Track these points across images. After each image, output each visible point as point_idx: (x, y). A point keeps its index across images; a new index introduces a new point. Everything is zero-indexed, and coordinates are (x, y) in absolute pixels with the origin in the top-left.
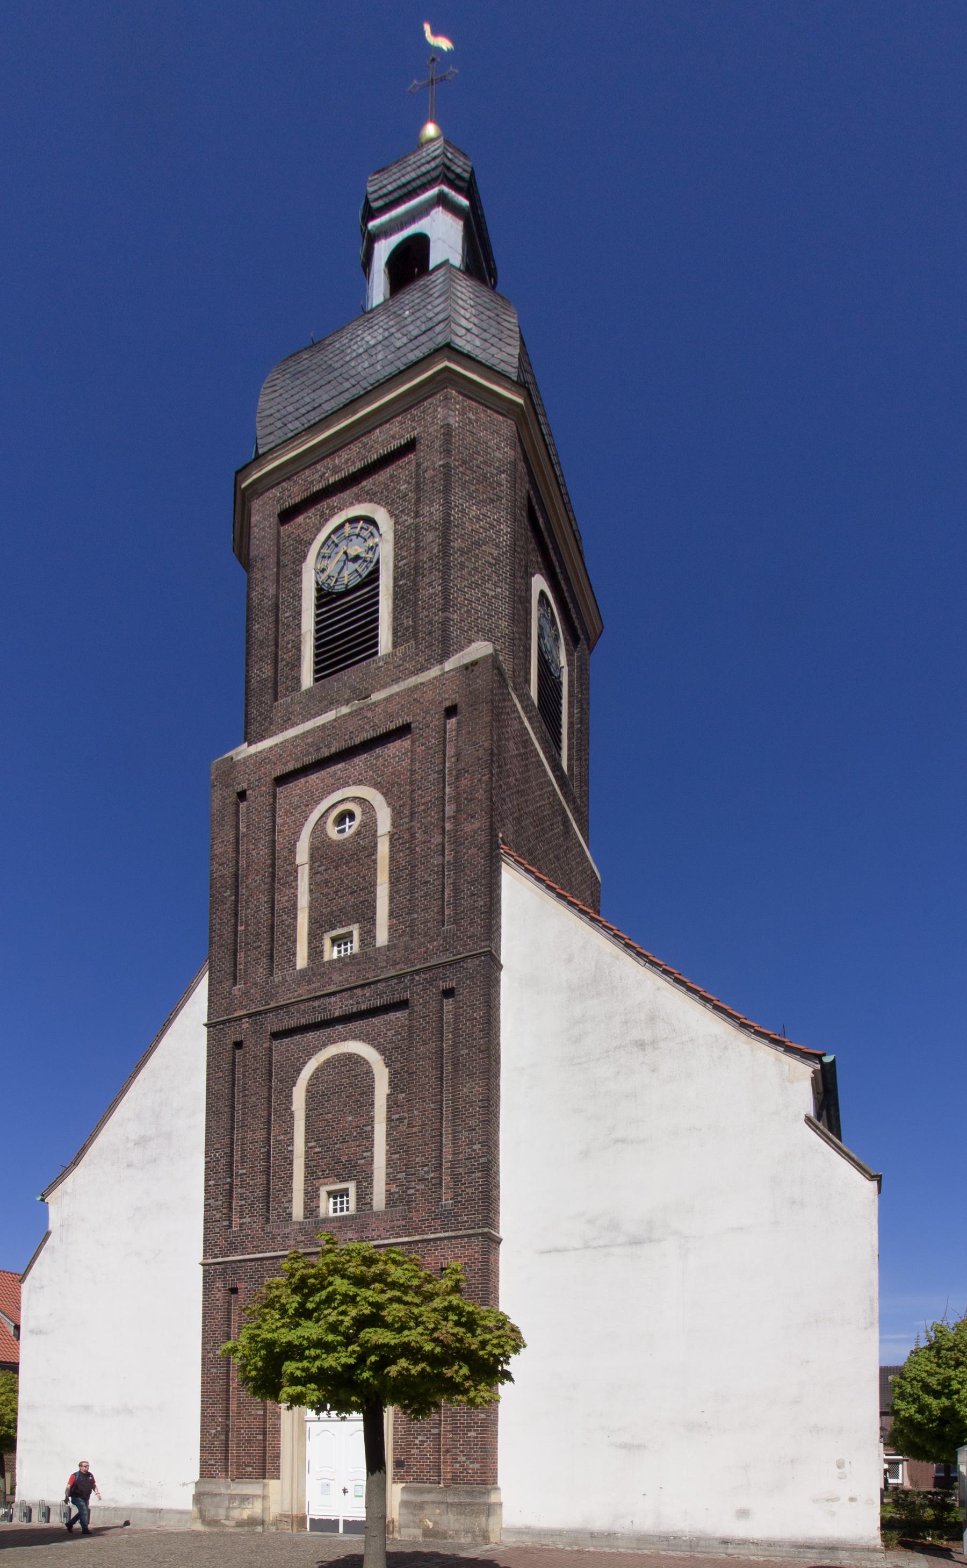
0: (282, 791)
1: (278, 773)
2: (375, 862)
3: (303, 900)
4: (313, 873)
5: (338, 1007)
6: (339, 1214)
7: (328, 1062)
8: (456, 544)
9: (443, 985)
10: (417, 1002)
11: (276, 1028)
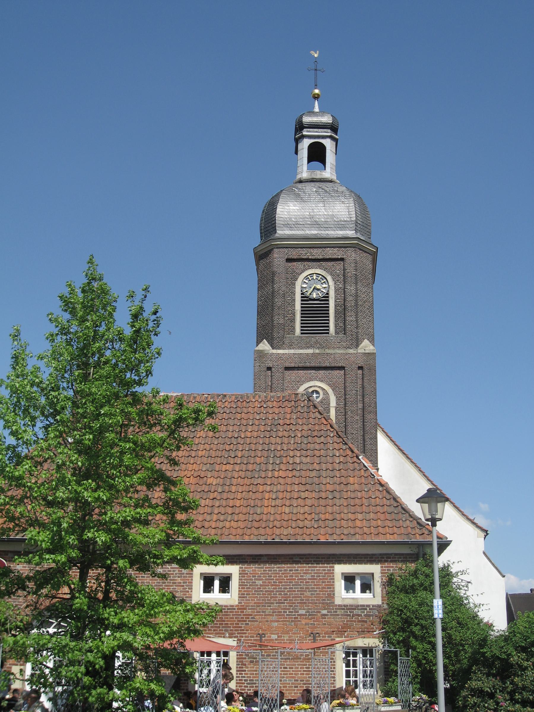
0: (287, 373)
1: (287, 365)
8: (360, 303)
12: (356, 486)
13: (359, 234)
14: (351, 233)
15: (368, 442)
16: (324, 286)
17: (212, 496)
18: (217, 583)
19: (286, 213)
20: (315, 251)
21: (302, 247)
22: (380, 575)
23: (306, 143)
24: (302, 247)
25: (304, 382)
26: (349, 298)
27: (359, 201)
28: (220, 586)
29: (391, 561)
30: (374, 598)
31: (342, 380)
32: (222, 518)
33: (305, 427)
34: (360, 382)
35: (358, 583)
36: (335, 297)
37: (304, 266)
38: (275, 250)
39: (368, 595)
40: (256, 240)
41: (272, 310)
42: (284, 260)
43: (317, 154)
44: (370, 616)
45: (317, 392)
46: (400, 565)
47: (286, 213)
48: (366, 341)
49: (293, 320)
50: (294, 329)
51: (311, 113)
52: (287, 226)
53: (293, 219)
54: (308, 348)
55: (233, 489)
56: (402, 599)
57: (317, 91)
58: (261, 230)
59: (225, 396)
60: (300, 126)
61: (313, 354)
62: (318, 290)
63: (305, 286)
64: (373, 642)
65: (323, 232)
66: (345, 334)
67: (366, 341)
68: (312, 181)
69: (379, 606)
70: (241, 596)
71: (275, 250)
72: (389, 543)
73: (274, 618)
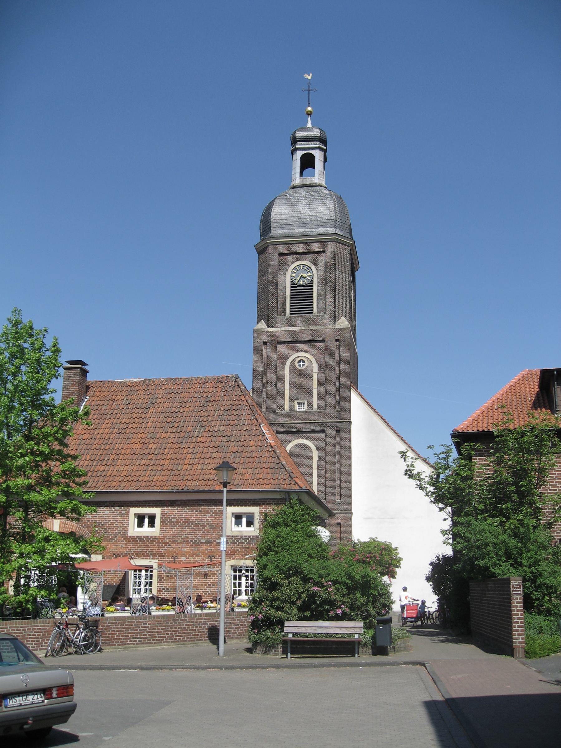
0: (280, 346)
2: (312, 380)
3: (287, 386)
4: (291, 378)
5: (301, 428)
6: (300, 410)
7: (296, 445)
9: (338, 428)
10: (328, 433)
11: (278, 430)
12: (253, 448)
13: (338, 230)
14: (331, 230)
15: (343, 400)
16: (310, 274)
17: (150, 457)
18: (146, 520)
19: (278, 216)
20: (302, 245)
21: (292, 243)
22: (259, 514)
23: (299, 154)
24: (292, 243)
25: (293, 353)
26: (329, 284)
27: (340, 202)
28: (149, 523)
29: (267, 504)
30: (254, 531)
31: (323, 350)
32: (153, 473)
33: (228, 403)
34: (337, 352)
35: (244, 520)
36: (318, 283)
37: (293, 258)
38: (271, 247)
39: (251, 529)
40: (257, 239)
41: (268, 296)
42: (277, 254)
43: (308, 162)
44: (251, 543)
45: (303, 361)
46: (273, 507)
47: (278, 216)
48: (343, 318)
49: (284, 304)
50: (285, 310)
51: (304, 128)
52: (280, 226)
53: (285, 221)
54: (296, 325)
55: (166, 451)
56: (273, 533)
57: (309, 109)
58: (260, 230)
59: (176, 379)
60: (295, 141)
61: (300, 331)
62: (305, 278)
63: (293, 275)
64: (249, 563)
65: (308, 230)
66: (325, 313)
67: (343, 318)
68: (303, 186)
69: (257, 537)
70: (162, 530)
71: (270, 246)
72: (263, 491)
73: (184, 545)
